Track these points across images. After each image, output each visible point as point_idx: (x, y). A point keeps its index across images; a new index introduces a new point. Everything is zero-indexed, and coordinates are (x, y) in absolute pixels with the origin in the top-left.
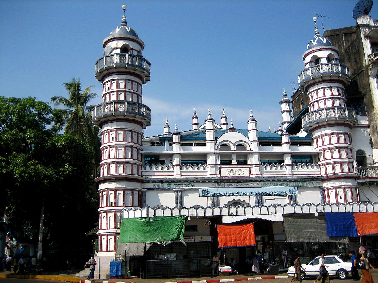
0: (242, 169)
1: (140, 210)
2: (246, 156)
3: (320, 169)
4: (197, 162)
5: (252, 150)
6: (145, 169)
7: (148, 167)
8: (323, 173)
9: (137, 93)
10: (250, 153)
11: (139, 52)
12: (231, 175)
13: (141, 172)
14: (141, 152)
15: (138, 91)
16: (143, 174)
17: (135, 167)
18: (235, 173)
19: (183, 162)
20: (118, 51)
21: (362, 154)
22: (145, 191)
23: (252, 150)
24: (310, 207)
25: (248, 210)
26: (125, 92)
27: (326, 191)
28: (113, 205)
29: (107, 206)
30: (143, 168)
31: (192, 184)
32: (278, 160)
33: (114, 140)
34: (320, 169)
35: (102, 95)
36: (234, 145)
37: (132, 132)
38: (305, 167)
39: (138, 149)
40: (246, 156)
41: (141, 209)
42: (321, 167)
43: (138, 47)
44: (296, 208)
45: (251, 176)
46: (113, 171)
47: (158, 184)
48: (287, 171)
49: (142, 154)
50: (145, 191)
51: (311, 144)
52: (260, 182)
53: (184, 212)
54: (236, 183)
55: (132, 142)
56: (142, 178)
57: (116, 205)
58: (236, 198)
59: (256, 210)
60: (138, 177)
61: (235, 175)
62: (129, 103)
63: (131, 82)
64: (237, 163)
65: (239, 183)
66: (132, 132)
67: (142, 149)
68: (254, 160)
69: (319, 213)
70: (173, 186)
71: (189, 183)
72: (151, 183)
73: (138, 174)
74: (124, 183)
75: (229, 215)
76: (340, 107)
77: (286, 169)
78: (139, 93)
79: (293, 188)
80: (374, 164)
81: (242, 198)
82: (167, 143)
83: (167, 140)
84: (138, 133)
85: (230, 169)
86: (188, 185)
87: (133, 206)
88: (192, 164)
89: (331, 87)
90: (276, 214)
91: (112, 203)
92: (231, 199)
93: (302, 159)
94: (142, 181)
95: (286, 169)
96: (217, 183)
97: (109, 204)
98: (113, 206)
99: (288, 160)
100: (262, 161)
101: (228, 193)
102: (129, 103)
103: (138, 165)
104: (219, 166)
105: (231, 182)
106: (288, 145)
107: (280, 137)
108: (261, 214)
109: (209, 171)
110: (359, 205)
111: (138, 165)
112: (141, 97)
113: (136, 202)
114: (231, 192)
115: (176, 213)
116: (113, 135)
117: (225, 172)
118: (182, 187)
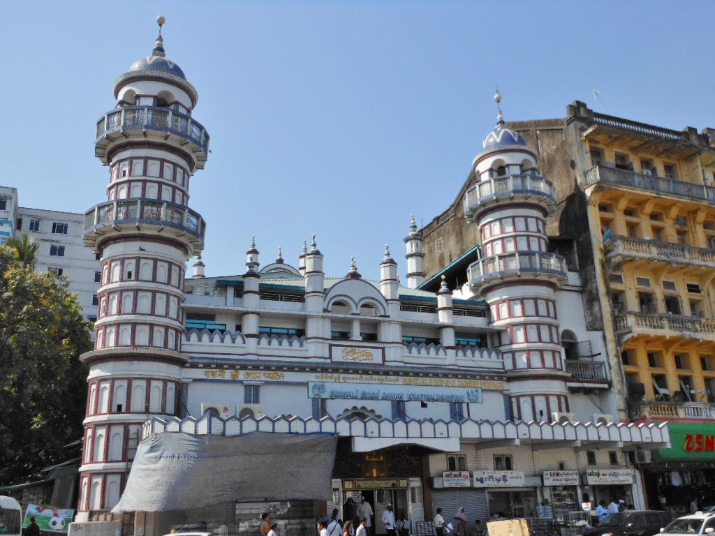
0: (369, 350)
1: (177, 421)
2: (376, 325)
3: (503, 359)
4: (268, 330)
5: (389, 317)
6: (188, 339)
7: (194, 336)
8: (509, 366)
9: (182, 188)
10: (384, 321)
11: (189, 111)
12: (349, 359)
13: (181, 345)
14: (182, 305)
15: (183, 186)
16: (184, 349)
17: (172, 333)
18: (356, 356)
19: (262, 330)
20: (150, 102)
21: (572, 338)
22: (187, 384)
23: (389, 317)
24: (323, 424)
25: (386, 427)
26: (515, 237)
27: (514, 400)
28: (124, 409)
29: (110, 412)
30: (184, 337)
31: (279, 373)
32: (433, 338)
33: (133, 278)
34: (503, 359)
35: (108, 187)
36: (357, 305)
37: (171, 264)
38: (423, 351)
39: (550, 326)
40: (376, 325)
41: (180, 420)
42: (505, 356)
43: (188, 103)
44: (244, 423)
45: (386, 364)
46: (126, 339)
47: (215, 370)
48: (450, 358)
49: (183, 308)
50: (187, 384)
51: (484, 313)
52: (402, 375)
53: (328, 427)
54: (358, 376)
55: (537, 315)
56: (183, 356)
57: (128, 411)
58: (359, 404)
59: (535, 428)
60: (176, 355)
61: (357, 361)
62: (522, 254)
63: (172, 166)
64: (361, 338)
65: (364, 376)
66: (171, 264)
67: (185, 299)
68: (391, 333)
69: (521, 439)
70: (242, 375)
71: (273, 370)
72: (201, 368)
73: (176, 349)
74: (111, 365)
75: (365, 436)
76: (505, 254)
77: (446, 355)
78: (184, 189)
79: (474, 390)
80: (593, 356)
81: (369, 405)
82: (231, 292)
83: (231, 286)
84: (180, 267)
85: (349, 349)
86: (271, 375)
87: (163, 412)
88: (279, 335)
89: (500, 220)
90: (448, 437)
91: (119, 407)
92: (349, 404)
93: (470, 340)
94: (181, 363)
95: (446, 355)
96: (324, 374)
97: (115, 409)
98: (124, 413)
99: (448, 338)
100: (405, 339)
101: (360, 391)
102: (522, 254)
103: (177, 331)
104: (331, 342)
105: (351, 373)
106: (257, 296)
107: (242, 279)
108: (421, 437)
109: (313, 350)
110: (517, 426)
111: (177, 331)
112: (188, 197)
113: (170, 407)
114: (367, 391)
115: (313, 427)
116: (131, 266)
117: (339, 355)
118: (261, 376)
